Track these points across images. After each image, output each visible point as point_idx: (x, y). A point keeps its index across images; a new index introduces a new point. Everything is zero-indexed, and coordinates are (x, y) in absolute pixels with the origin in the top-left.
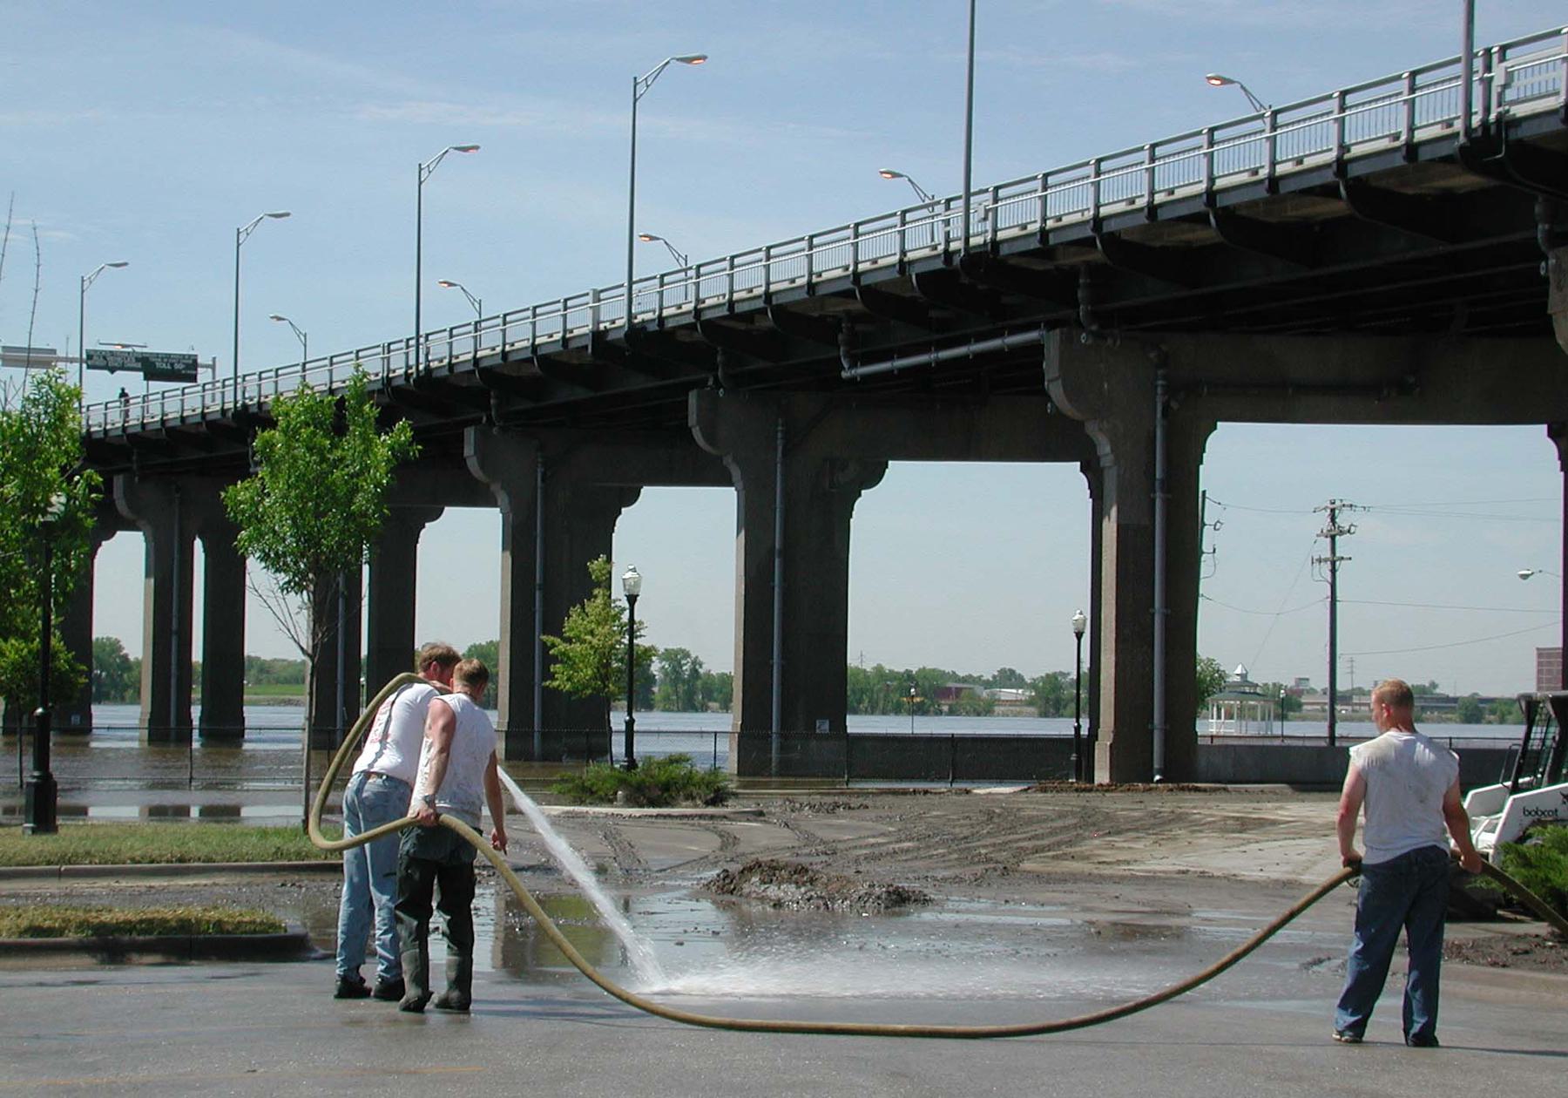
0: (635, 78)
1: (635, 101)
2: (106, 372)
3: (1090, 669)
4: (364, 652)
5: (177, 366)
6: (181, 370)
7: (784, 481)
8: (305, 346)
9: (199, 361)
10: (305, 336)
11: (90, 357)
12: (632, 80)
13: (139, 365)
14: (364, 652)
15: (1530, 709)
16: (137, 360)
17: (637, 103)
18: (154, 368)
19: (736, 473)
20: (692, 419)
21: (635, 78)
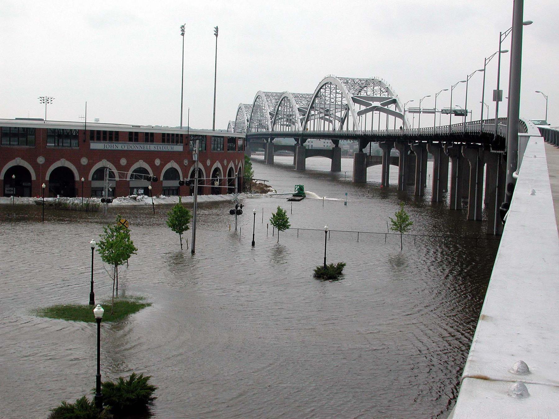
0: (501, 32)
1: (500, 43)
2: (446, 114)
3: (451, 205)
4: (450, 164)
5: (462, 112)
6: (462, 113)
7: (458, 165)
8: (547, 100)
9: (468, 111)
10: (547, 97)
11: (442, 111)
12: (499, 33)
13: (454, 112)
14: (450, 164)
15: (390, 195)
16: (453, 111)
17: (501, 44)
18: (457, 113)
19: (307, 138)
20: (427, 148)
21: (501, 32)
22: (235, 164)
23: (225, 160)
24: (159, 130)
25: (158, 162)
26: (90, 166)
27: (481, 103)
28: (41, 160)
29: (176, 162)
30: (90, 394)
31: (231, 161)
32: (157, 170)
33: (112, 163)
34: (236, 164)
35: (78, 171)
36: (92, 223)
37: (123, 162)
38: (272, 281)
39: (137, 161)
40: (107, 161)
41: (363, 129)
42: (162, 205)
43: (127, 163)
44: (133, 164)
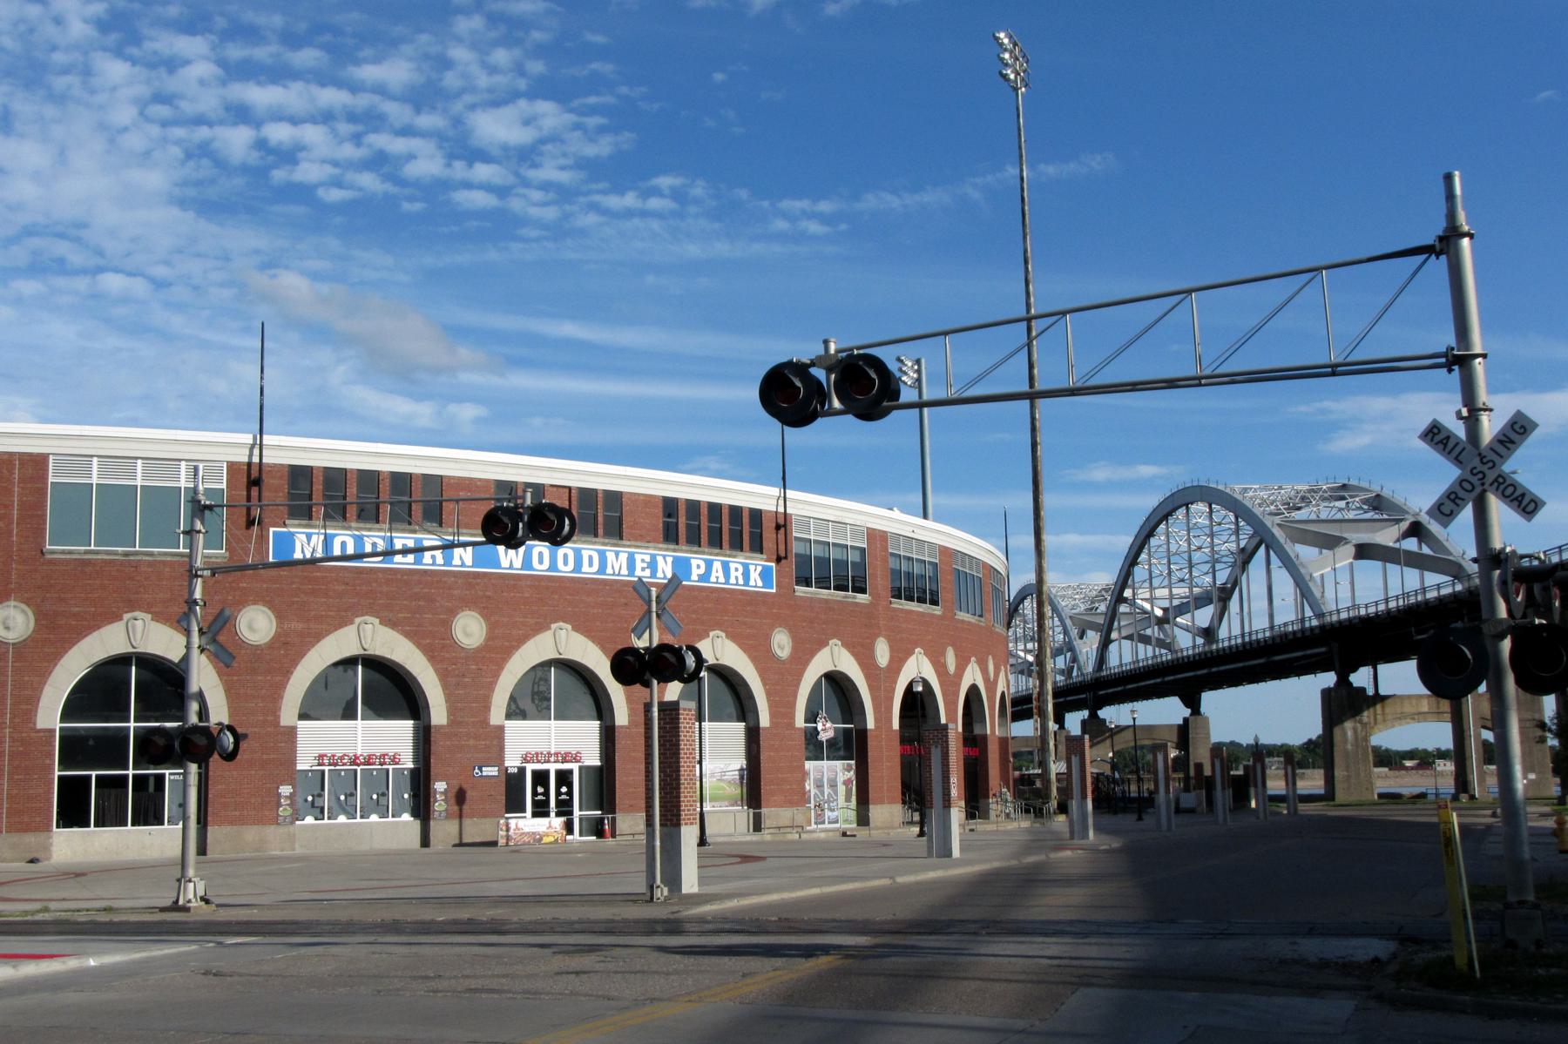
22: (984, 671)
23: (990, 657)
24: (415, 944)
25: (469, 629)
26: (287, 650)
27: (1239, 616)
28: (782, 644)
29: (732, 636)
30: (213, 903)
31: (973, 659)
32: (782, 677)
33: (407, 635)
34: (944, 666)
35: (443, 676)
36: (1236, 583)
37: (469, 629)
38: (229, 978)
39: (541, 627)
40: (727, 637)
41: (1345, 603)
42: (1038, 625)
43: (490, 637)
44: (318, 637)
